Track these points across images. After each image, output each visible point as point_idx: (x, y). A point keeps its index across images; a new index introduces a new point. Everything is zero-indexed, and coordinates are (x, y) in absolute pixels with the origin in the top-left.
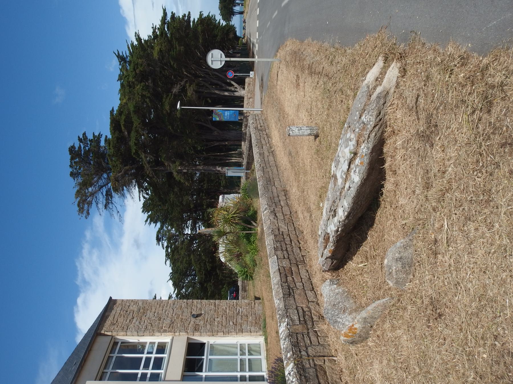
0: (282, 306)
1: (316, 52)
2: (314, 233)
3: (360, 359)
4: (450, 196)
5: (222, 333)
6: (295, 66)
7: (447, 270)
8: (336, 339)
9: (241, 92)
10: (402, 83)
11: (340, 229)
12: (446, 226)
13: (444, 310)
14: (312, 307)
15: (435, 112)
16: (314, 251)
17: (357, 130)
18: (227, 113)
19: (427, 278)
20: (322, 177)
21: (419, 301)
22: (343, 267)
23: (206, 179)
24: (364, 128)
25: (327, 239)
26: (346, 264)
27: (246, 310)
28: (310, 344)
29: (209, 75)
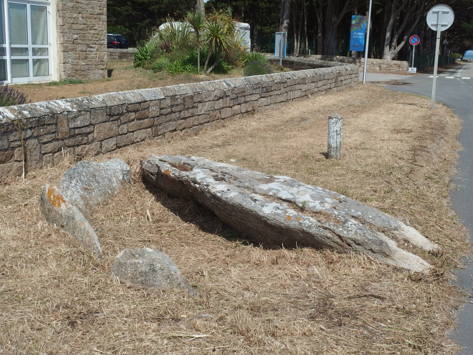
0: (95, 104)
1: (443, 157)
2: (195, 150)
3: (20, 210)
4: (240, 342)
5: (61, 24)
6: (424, 128)
7: (135, 335)
8: (50, 177)
9: (389, 54)
10: (401, 276)
11: (197, 186)
12: (198, 336)
13: (81, 330)
14: (93, 146)
15: (360, 323)
16: (170, 149)
17: (336, 213)
18: (361, 35)
19: (126, 306)
20: (271, 161)
21: (93, 294)
22: (147, 188)
23: (272, 6)
24: (338, 222)
25: (185, 167)
26: (150, 192)
27: (93, 58)
28: (42, 142)
29: (416, 11)
